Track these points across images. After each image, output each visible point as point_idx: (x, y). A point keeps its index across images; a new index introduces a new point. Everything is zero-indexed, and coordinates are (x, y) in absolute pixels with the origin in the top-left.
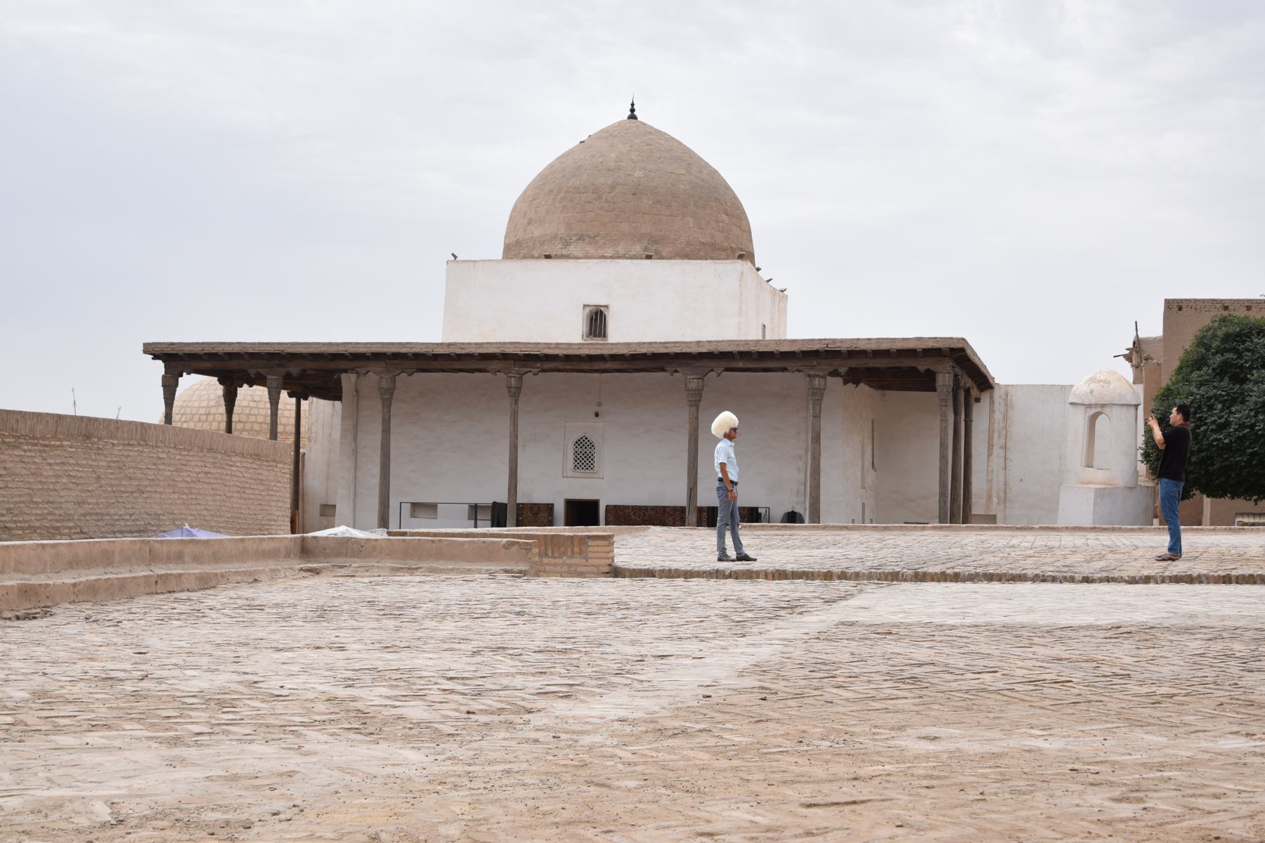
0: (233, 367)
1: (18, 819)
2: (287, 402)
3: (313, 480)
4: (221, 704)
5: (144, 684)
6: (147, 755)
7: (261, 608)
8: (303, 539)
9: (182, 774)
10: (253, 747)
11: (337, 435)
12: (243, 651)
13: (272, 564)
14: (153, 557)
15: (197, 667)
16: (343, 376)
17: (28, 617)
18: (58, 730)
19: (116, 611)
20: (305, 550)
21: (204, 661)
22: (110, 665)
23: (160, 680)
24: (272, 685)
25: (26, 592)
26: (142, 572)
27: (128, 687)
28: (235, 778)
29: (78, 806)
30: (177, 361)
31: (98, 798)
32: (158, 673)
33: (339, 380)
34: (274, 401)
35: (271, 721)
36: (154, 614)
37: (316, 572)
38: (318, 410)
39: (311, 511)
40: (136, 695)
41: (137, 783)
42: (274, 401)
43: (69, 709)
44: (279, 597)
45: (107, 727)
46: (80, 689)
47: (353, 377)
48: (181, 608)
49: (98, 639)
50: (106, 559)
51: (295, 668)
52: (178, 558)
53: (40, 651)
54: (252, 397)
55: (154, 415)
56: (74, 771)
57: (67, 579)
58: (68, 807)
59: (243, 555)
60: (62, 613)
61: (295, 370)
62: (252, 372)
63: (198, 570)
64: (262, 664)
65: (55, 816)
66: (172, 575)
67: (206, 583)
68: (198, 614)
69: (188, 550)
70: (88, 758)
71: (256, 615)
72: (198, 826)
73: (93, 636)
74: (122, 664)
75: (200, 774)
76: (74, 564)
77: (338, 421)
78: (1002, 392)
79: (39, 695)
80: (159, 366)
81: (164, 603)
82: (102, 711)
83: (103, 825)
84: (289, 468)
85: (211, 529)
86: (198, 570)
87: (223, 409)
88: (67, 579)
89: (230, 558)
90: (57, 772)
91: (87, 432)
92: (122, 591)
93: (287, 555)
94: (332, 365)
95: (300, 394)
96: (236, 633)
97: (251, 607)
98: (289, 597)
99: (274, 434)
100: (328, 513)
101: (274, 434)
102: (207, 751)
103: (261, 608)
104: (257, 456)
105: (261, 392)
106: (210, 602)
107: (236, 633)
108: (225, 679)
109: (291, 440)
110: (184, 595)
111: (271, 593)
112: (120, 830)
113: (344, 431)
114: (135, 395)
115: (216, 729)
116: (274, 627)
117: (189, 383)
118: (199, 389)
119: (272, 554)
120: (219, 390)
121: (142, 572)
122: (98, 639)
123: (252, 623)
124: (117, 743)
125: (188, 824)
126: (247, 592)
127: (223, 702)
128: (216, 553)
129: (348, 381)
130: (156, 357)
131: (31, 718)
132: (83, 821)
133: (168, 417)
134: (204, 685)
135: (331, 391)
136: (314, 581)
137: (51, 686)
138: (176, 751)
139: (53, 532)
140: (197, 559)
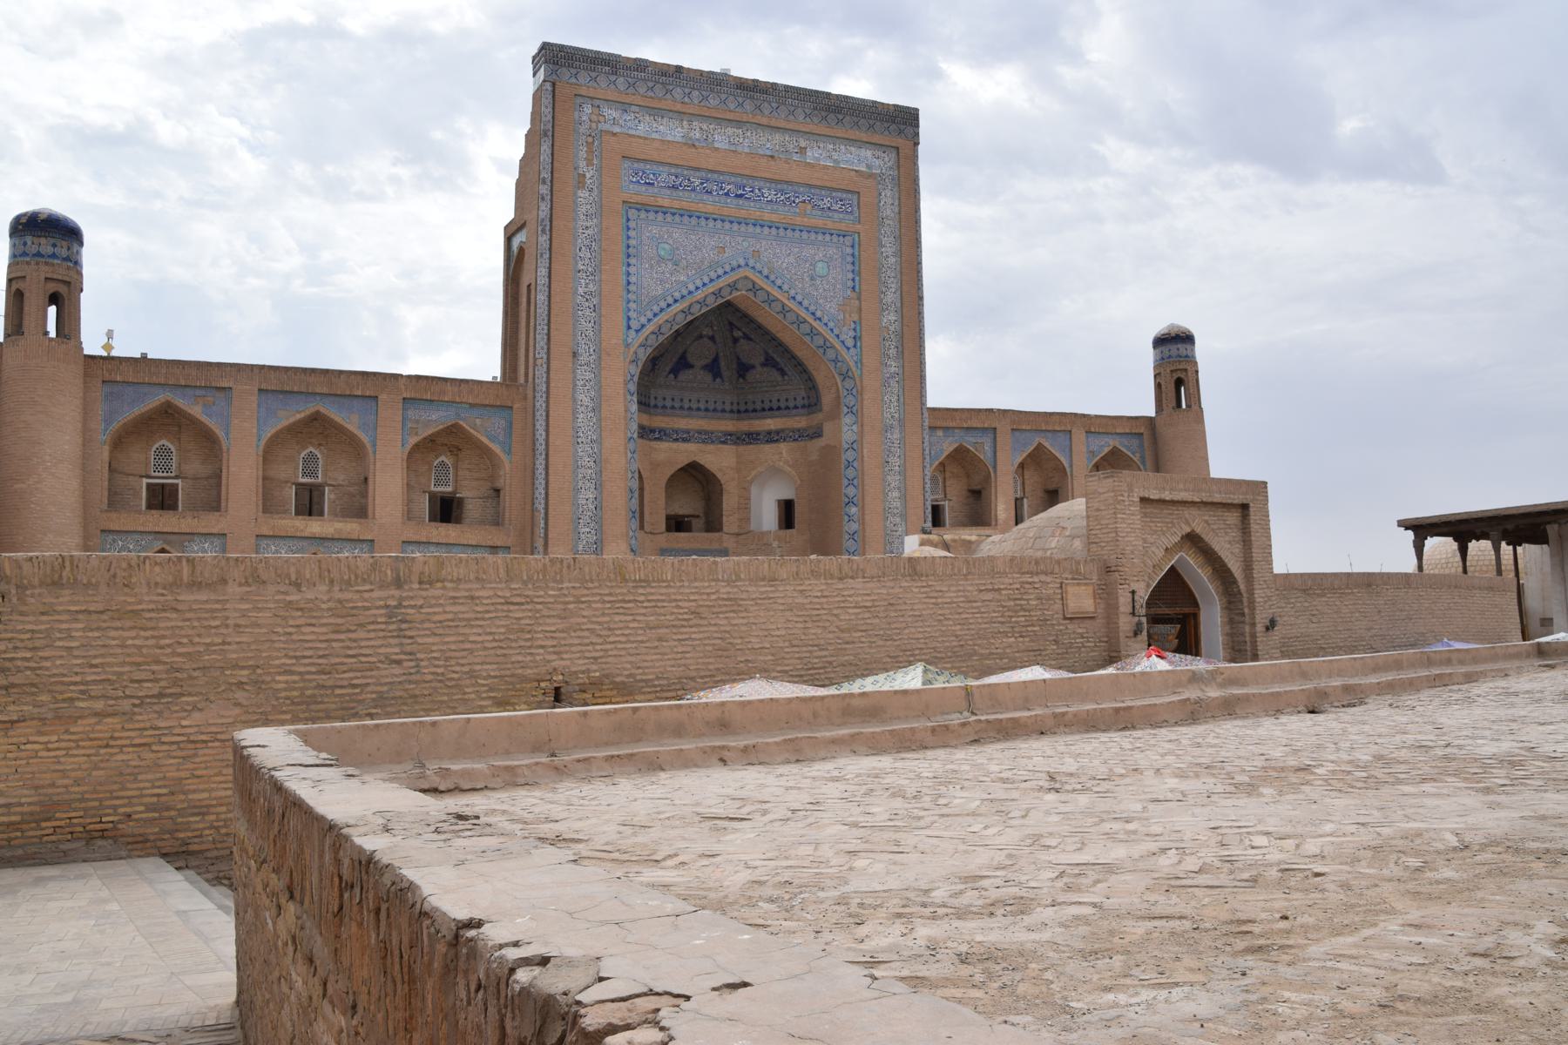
0: (1463, 529)
1: (1393, 842)
2: (1506, 549)
3: (1533, 602)
4: (1512, 764)
5: (1449, 750)
6: (1472, 800)
7: (1516, 694)
8: (1539, 644)
9: (1502, 814)
10: (1548, 795)
11: (1547, 569)
12: (1514, 726)
13: (1517, 663)
14: (1430, 662)
15: (1483, 738)
16: (1548, 527)
17: (1349, 706)
18: (1400, 782)
19: (1409, 699)
20: (1541, 651)
21: (1487, 733)
22: (1419, 737)
23: (1460, 747)
24: (1547, 749)
25: (1347, 689)
26: (1424, 673)
27: (1440, 752)
28: (1543, 818)
29: (1432, 834)
30: (1422, 529)
31: (1446, 829)
32: (1456, 742)
33: (1545, 531)
34: (1497, 549)
35: (1554, 776)
36: (1437, 702)
37: (1552, 667)
38: (1528, 552)
39: (1534, 624)
40: (1445, 757)
41: (1470, 820)
42: (1497, 549)
43: (1403, 768)
44: (1528, 687)
45: (1435, 780)
46: (1404, 754)
47: (1556, 526)
48: (1456, 696)
49: (1404, 719)
50: (1398, 665)
51: (1561, 737)
52: (1449, 662)
53: (1366, 728)
54: (1480, 548)
55: (1408, 564)
56: (1421, 810)
57: (1373, 679)
58: (1426, 836)
59: (1495, 658)
60: (1372, 702)
61: (1510, 527)
62: (1478, 531)
63: (1463, 669)
64: (1533, 734)
65: (1418, 841)
66: (1444, 675)
67: (1470, 678)
68: (1469, 701)
69: (1454, 656)
70: (1429, 802)
71: (1513, 699)
72: (1526, 852)
73: (1401, 718)
74: (1428, 737)
75: (1516, 815)
76: (1376, 669)
77: (1547, 559)
78: (1183, 351)
79: (1378, 757)
80: (1410, 534)
81: (1445, 694)
82: (1427, 769)
83: (1455, 849)
84: (1515, 595)
85: (1463, 640)
86: (1463, 669)
87: (1458, 558)
88: (1373, 679)
89: (1485, 660)
90: (1410, 811)
91: (1368, 582)
92: (1412, 686)
93: (1528, 656)
94: (1538, 520)
95: (1515, 542)
96: (1502, 713)
97: (1508, 694)
98: (1536, 686)
99: (1499, 572)
100: (1547, 624)
101: (1499, 572)
102: (1515, 798)
103: (1516, 694)
104: (1491, 589)
105: (1486, 544)
106: (1476, 691)
107: (1502, 713)
108: (1506, 746)
109: (1512, 574)
110: (1455, 687)
111: (1522, 683)
112: (1466, 853)
113: (1553, 566)
114: (1397, 555)
115: (1514, 782)
116: (1530, 708)
117: (1431, 543)
118: (1440, 547)
119: (1517, 656)
120: (1455, 545)
121: (1424, 673)
122: (1404, 719)
123: (1513, 705)
124: (1445, 791)
125: (1517, 850)
126: (1502, 683)
127: (1512, 763)
128: (1475, 658)
129: (1552, 530)
130: (1407, 528)
131: (1379, 773)
132: (1440, 846)
133: (1420, 567)
134: (1495, 750)
135: (1539, 538)
136: (1552, 673)
137: (1385, 752)
138: (1491, 798)
139: (1353, 649)
140: (1462, 662)
